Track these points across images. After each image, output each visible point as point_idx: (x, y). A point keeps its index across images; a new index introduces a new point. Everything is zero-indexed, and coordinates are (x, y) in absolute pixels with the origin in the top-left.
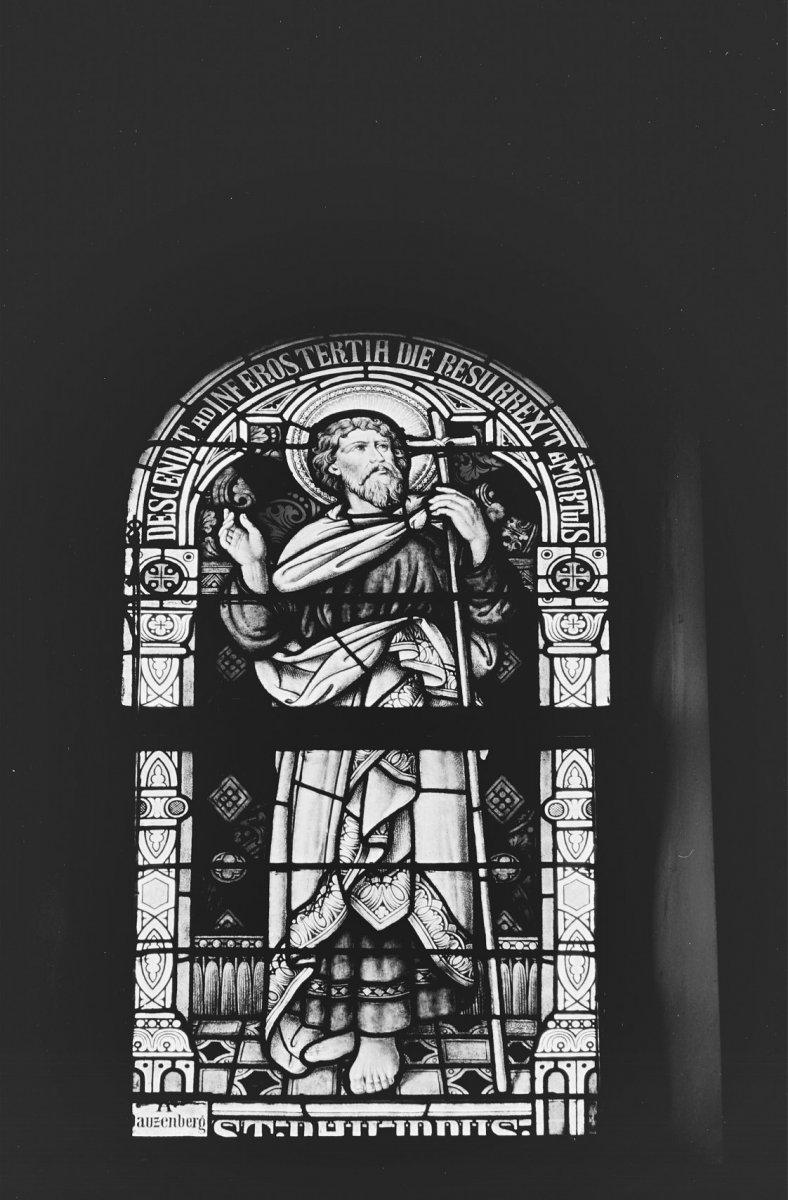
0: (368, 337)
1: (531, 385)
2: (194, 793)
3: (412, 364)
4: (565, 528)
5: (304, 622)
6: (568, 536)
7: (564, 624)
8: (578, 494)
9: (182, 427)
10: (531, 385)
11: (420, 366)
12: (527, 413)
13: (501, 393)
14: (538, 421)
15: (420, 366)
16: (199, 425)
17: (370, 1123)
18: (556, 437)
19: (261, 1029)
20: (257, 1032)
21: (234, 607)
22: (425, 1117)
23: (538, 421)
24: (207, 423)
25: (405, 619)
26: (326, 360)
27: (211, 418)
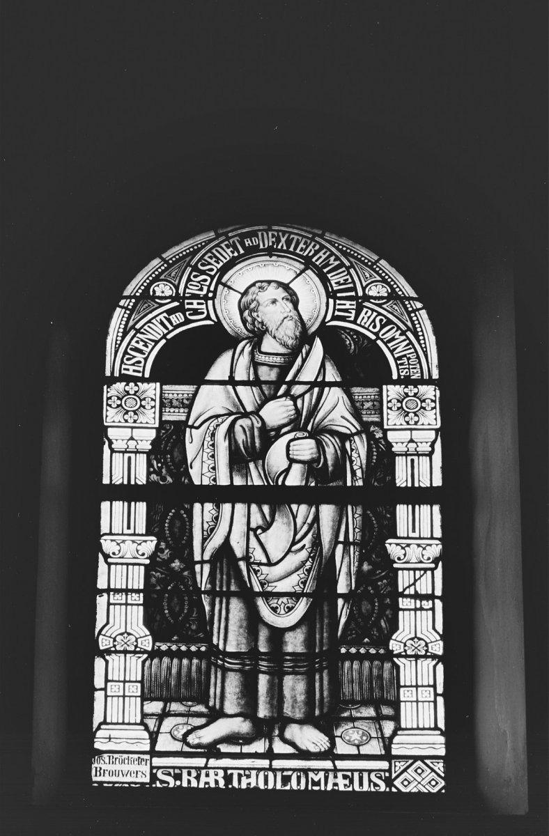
0: (281, 231)
1: (325, 683)
2: (342, 374)
3: (366, 326)
4: (369, 326)
5: (353, 347)
6: (375, 327)
7: (127, 388)
8: (366, 314)
9: (237, 238)
10: (325, 683)
11: (298, 251)
12: (274, 240)
13: (363, 318)
14: (283, 240)
15: (298, 251)
16: (247, 243)
17: (364, 773)
18: (293, 238)
19: (378, 447)
20: (377, 397)
21: (248, 345)
22: (206, 767)
23: (283, 240)
24: (251, 244)
25: (339, 633)
26: (301, 250)
27: (255, 244)
